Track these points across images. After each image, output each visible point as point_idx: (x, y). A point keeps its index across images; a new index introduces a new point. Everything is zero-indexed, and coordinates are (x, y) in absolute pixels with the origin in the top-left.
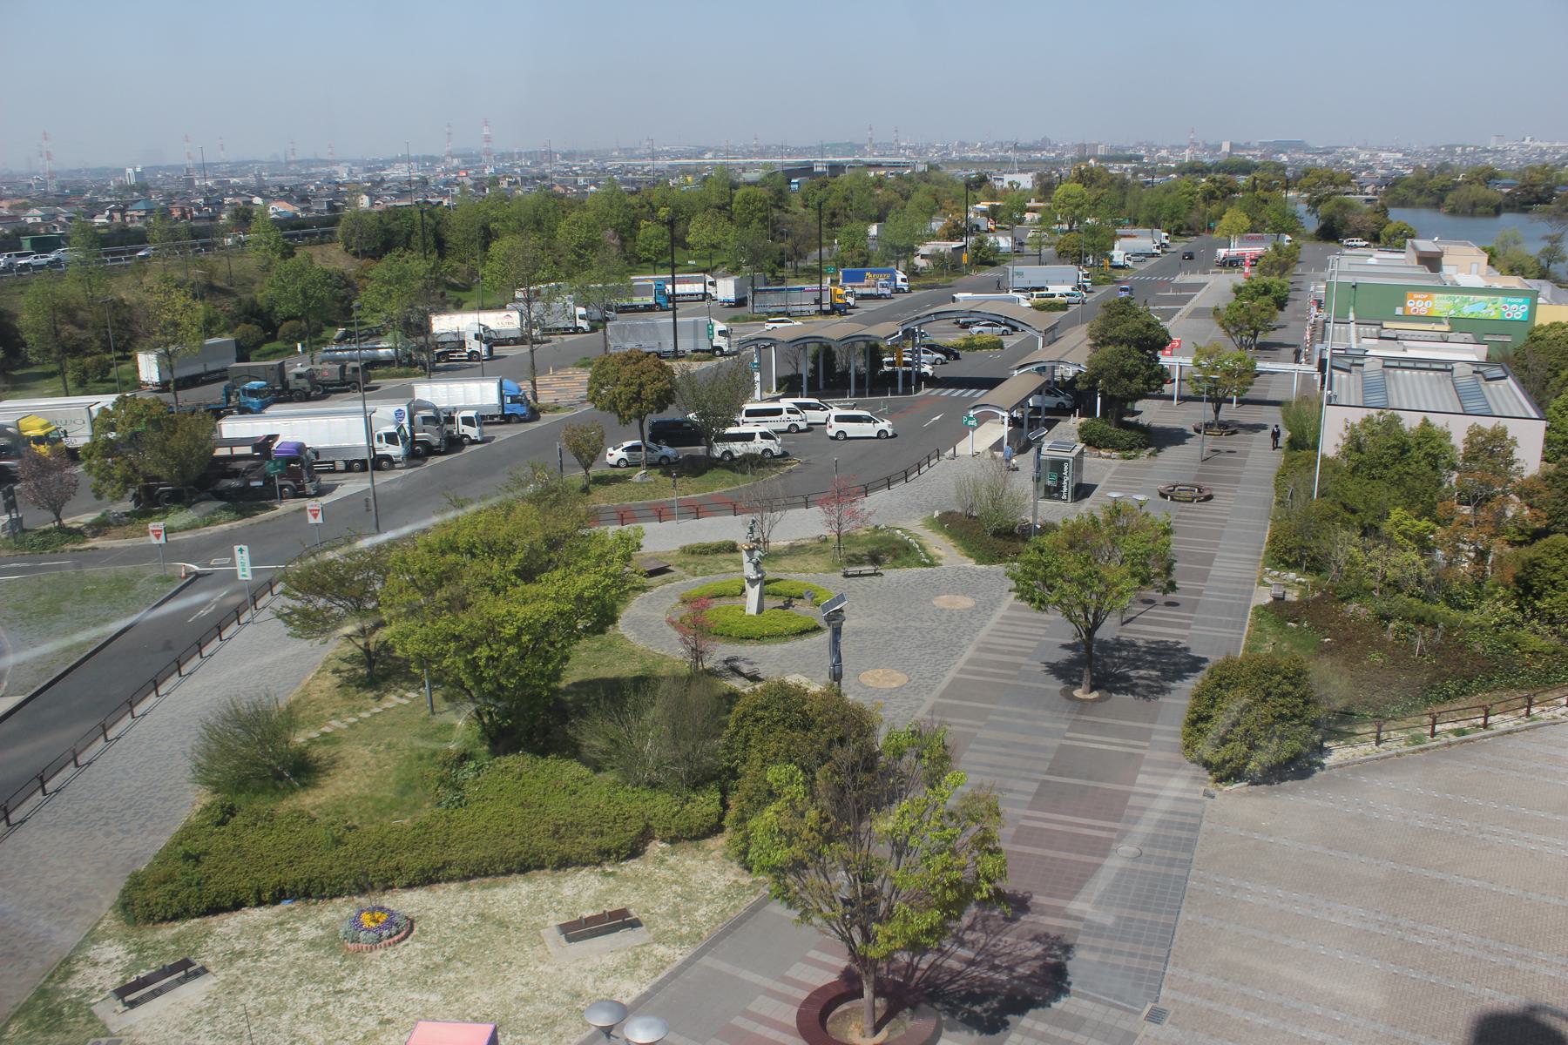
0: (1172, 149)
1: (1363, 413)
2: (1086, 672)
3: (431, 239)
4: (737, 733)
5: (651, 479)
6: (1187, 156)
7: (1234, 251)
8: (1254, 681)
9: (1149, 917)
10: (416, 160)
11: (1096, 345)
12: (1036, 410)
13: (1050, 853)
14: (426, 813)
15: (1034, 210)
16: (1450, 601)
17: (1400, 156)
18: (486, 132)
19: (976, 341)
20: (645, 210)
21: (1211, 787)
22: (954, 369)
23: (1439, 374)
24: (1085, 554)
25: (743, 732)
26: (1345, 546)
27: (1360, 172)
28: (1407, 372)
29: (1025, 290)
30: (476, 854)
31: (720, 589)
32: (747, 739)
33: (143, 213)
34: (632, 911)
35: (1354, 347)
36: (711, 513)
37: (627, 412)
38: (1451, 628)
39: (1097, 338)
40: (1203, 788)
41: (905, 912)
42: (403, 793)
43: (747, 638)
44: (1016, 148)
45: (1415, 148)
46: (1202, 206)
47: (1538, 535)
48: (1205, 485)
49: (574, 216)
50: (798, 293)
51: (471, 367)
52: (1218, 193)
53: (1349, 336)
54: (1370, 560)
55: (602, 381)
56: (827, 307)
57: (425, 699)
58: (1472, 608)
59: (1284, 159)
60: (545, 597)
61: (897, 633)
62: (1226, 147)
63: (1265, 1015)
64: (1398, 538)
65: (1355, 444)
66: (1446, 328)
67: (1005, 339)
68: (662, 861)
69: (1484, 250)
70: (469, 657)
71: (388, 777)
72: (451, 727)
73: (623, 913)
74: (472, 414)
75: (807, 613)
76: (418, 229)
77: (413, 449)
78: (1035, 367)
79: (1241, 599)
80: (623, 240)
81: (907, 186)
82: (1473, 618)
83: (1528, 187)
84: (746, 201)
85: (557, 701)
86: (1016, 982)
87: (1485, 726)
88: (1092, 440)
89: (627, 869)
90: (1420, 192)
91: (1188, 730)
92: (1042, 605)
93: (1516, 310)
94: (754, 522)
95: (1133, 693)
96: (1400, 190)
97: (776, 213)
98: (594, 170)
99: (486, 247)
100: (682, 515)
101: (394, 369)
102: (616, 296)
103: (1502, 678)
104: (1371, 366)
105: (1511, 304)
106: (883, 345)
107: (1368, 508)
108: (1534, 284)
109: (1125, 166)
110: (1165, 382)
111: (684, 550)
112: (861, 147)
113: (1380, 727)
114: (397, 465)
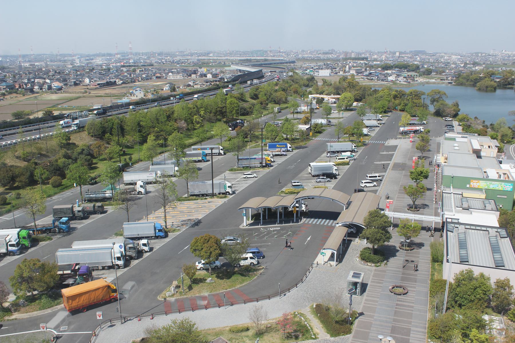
17: (459, 57)
18: (130, 46)
23: (484, 232)
28: (473, 231)
33: (5, 87)
45: (464, 53)
46: (393, 100)
50: (254, 160)
52: (398, 96)
56: (264, 165)
77: (126, 259)
83: (505, 79)
90: (468, 80)
96: (461, 79)
105: (506, 185)
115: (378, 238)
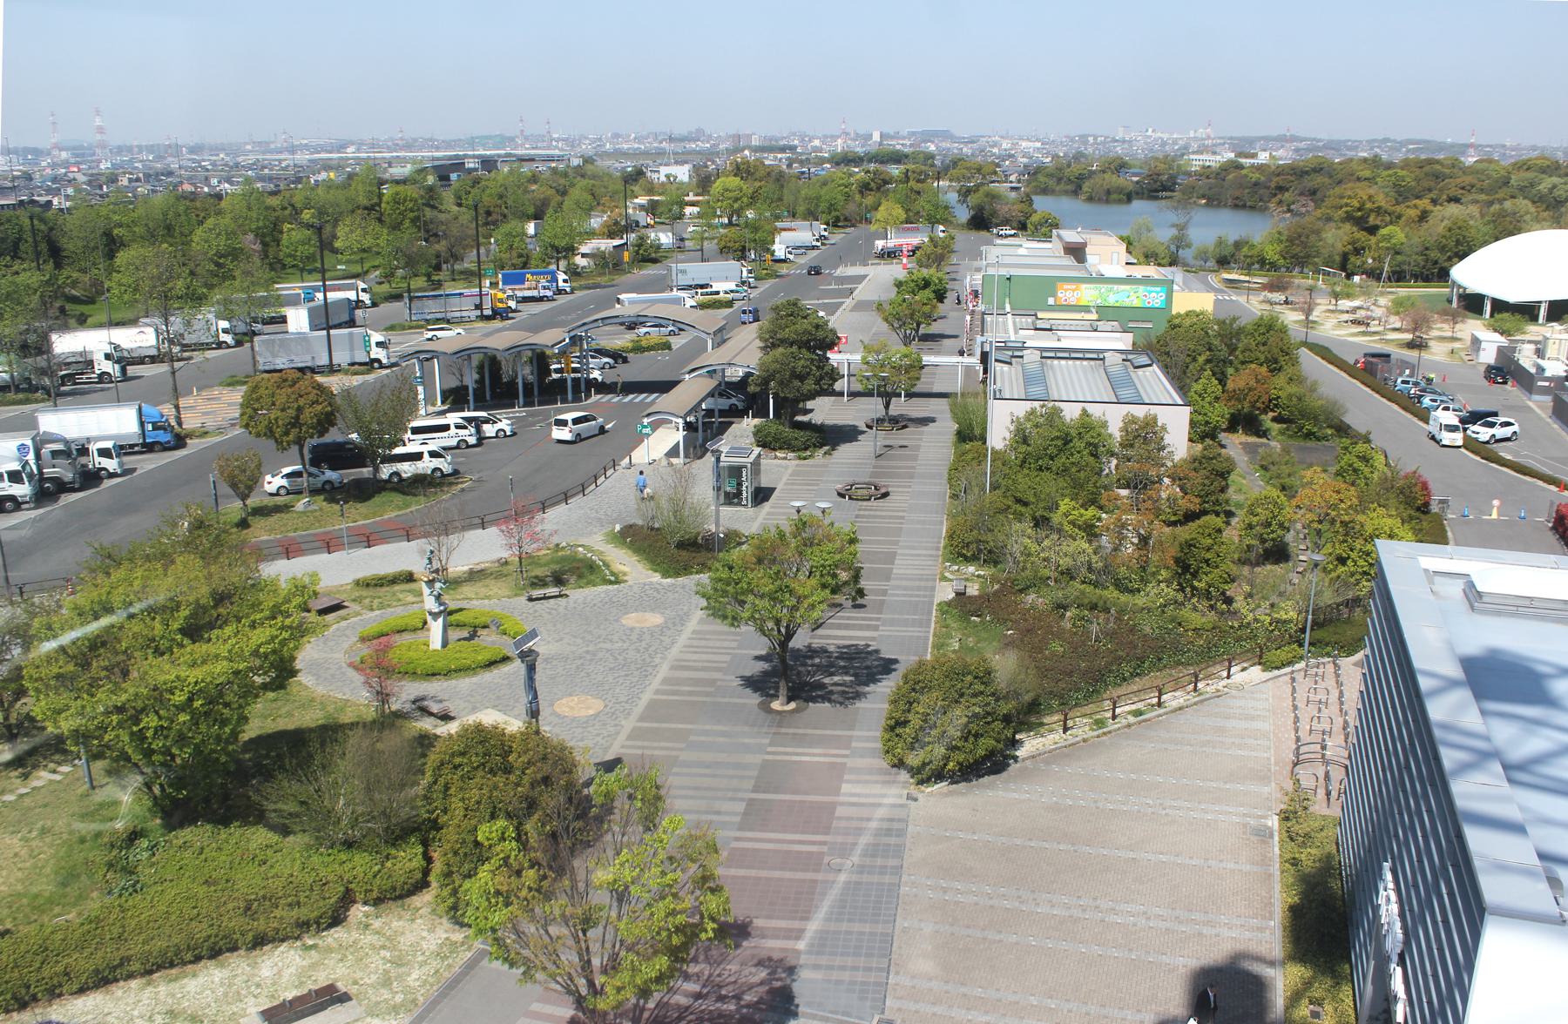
0: (824, 139)
1: (1027, 406)
2: (782, 684)
3: (43, 247)
4: (435, 782)
5: (315, 507)
6: (839, 146)
7: (892, 242)
8: (947, 684)
9: (867, 928)
10: (15, 151)
11: (767, 347)
12: (710, 413)
13: (764, 873)
14: (95, 903)
15: (693, 204)
16: (1120, 585)
17: (1038, 145)
18: (98, 122)
19: (644, 343)
20: (287, 212)
21: (913, 790)
22: (626, 373)
23: (1092, 363)
24: (775, 568)
25: (442, 781)
26: (1020, 537)
27: (1004, 160)
29: (690, 287)
30: (160, 944)
31: (401, 623)
32: (447, 788)
34: (339, 985)
35: (1013, 339)
36: (383, 540)
37: (285, 438)
38: (1121, 612)
39: (766, 340)
40: (906, 792)
41: (632, 961)
42: (64, 885)
43: (434, 675)
44: (671, 139)
46: (858, 197)
47: (1190, 517)
48: (881, 482)
49: (210, 222)
50: (456, 300)
51: (102, 390)
53: (1007, 328)
54: (1043, 550)
55: (256, 406)
56: (488, 312)
57: (82, 772)
58: (1139, 591)
59: (932, 148)
60: (217, 656)
61: (589, 657)
62: (876, 137)
63: (986, 1012)
64: (1067, 527)
65: (1021, 437)
66: (1094, 316)
67: (672, 339)
68: (367, 926)
69: (1122, 238)
70: (135, 729)
71: (43, 867)
72: (116, 803)
73: (331, 988)
74: (109, 444)
75: (493, 643)
76: (28, 236)
77: (41, 487)
78: (705, 370)
79: (925, 596)
80: (265, 244)
81: (562, 181)
82: (1140, 600)
83: (1154, 176)
84: (396, 201)
85: (238, 762)
86: (745, 1010)
87: (1159, 704)
88: (766, 442)
89: (330, 940)
90: (1060, 180)
91: (887, 736)
92: (735, 620)
93: (1154, 298)
94: (432, 552)
95: (830, 701)
96: (1041, 178)
97: (428, 213)
98: (226, 165)
99: (111, 255)
100: (352, 545)
101: (11, 396)
102: (265, 305)
103: (1170, 656)
104: (1031, 357)
105: (1150, 292)
106: (548, 352)
107: (1039, 500)
108: (1167, 272)
109: (779, 156)
110: (836, 380)
111: (357, 583)
112: (512, 139)
113: (1066, 715)
114: (24, 506)
115: (798, 370)
